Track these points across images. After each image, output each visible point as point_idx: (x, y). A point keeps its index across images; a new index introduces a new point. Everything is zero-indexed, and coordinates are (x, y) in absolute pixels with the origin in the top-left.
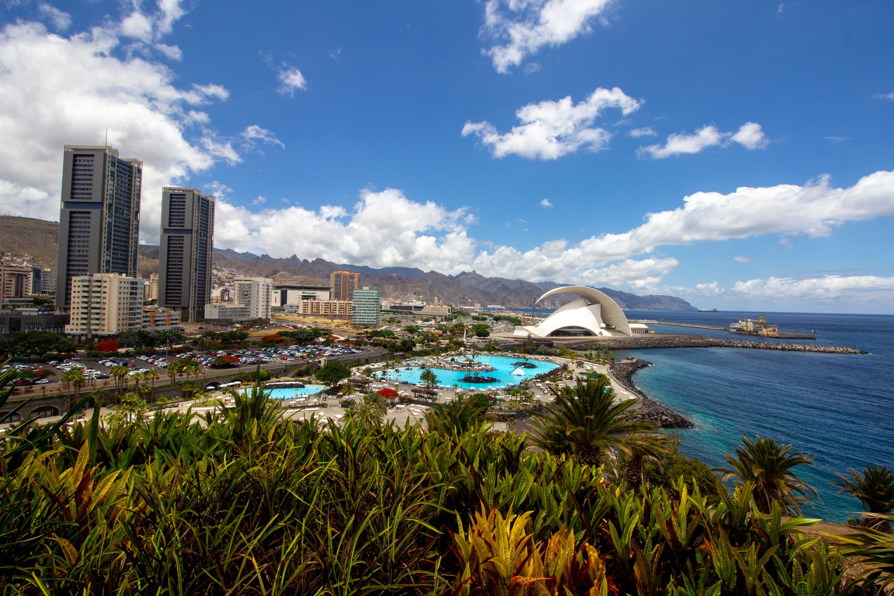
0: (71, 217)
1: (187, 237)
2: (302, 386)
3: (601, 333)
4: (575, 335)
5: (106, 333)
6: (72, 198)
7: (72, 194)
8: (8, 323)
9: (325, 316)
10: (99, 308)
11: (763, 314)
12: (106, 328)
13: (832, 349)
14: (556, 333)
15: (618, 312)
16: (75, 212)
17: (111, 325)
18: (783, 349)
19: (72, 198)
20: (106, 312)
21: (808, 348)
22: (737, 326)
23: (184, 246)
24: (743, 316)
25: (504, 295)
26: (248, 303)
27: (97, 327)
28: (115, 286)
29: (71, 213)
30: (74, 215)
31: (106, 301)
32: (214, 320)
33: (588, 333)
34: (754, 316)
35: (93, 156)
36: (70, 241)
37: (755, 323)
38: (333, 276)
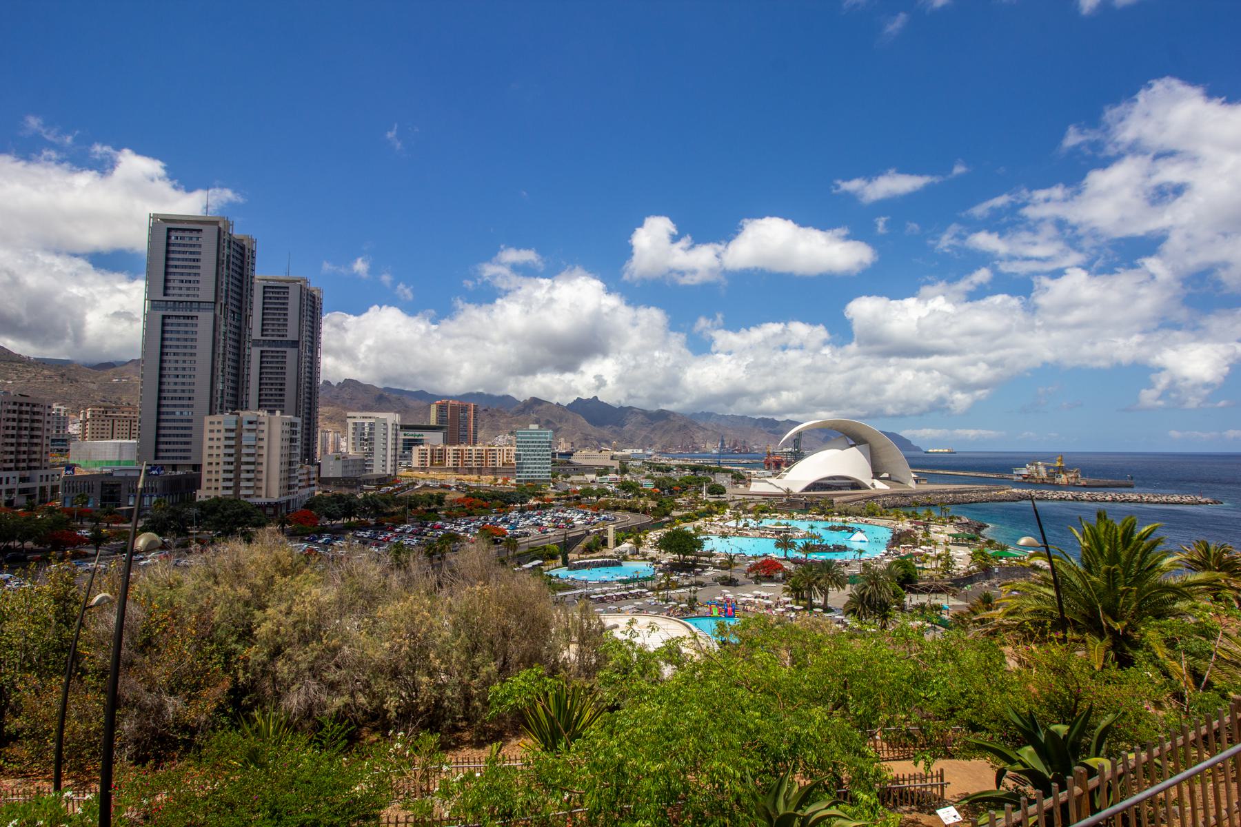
0: (164, 324)
1: (291, 353)
2: (619, 564)
3: (873, 485)
4: (839, 488)
5: (263, 500)
6: (165, 295)
7: (166, 288)
8: (98, 490)
9: (456, 470)
10: (253, 463)
11: (1062, 456)
12: (263, 493)
13: (1177, 498)
14: (815, 486)
15: (897, 460)
16: (169, 317)
17: (272, 490)
18: (1114, 500)
19: (165, 295)
20: (264, 468)
21: (1145, 498)
22: (1024, 472)
23: (287, 366)
24: (1032, 459)
25: (644, 433)
26: (371, 453)
27: (250, 492)
28: (277, 429)
29: (164, 317)
30: (167, 321)
31: (264, 452)
32: (335, 479)
33: (856, 485)
34: (1047, 458)
36: (162, 361)
37: (1047, 468)
38: (434, 408)
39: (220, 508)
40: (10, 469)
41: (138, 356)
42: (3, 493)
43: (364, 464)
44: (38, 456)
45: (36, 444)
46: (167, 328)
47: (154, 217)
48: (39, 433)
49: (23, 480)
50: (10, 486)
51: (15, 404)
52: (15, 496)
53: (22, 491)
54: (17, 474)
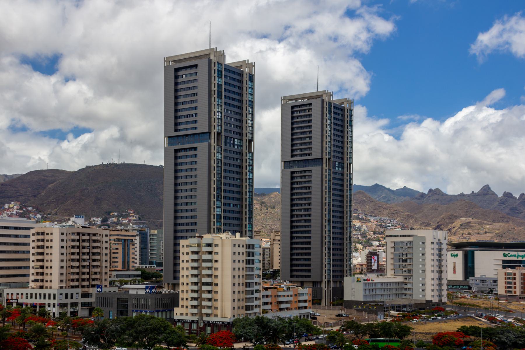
5: (219, 319)
12: (219, 312)
27: (208, 311)
30: (180, 154)
32: (358, 303)
35: (196, 66)
39: (136, 325)
40: (77, 287)
41: (278, 187)
42: (69, 306)
43: (402, 288)
44: (98, 276)
45: (97, 267)
46: (180, 161)
47: (167, 60)
48: (98, 257)
49: (85, 295)
50: (74, 300)
51: (78, 234)
52: (79, 308)
53: (84, 305)
54: (80, 290)
